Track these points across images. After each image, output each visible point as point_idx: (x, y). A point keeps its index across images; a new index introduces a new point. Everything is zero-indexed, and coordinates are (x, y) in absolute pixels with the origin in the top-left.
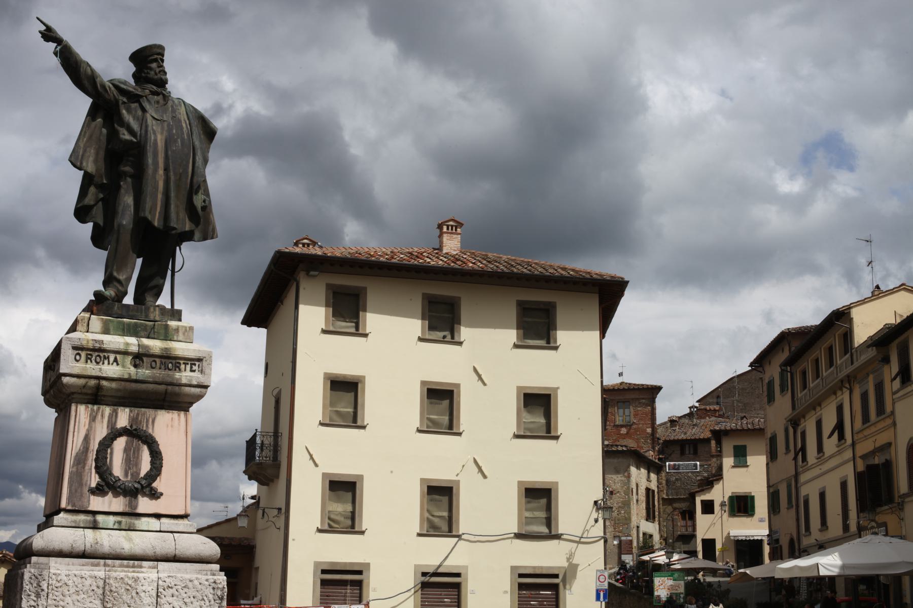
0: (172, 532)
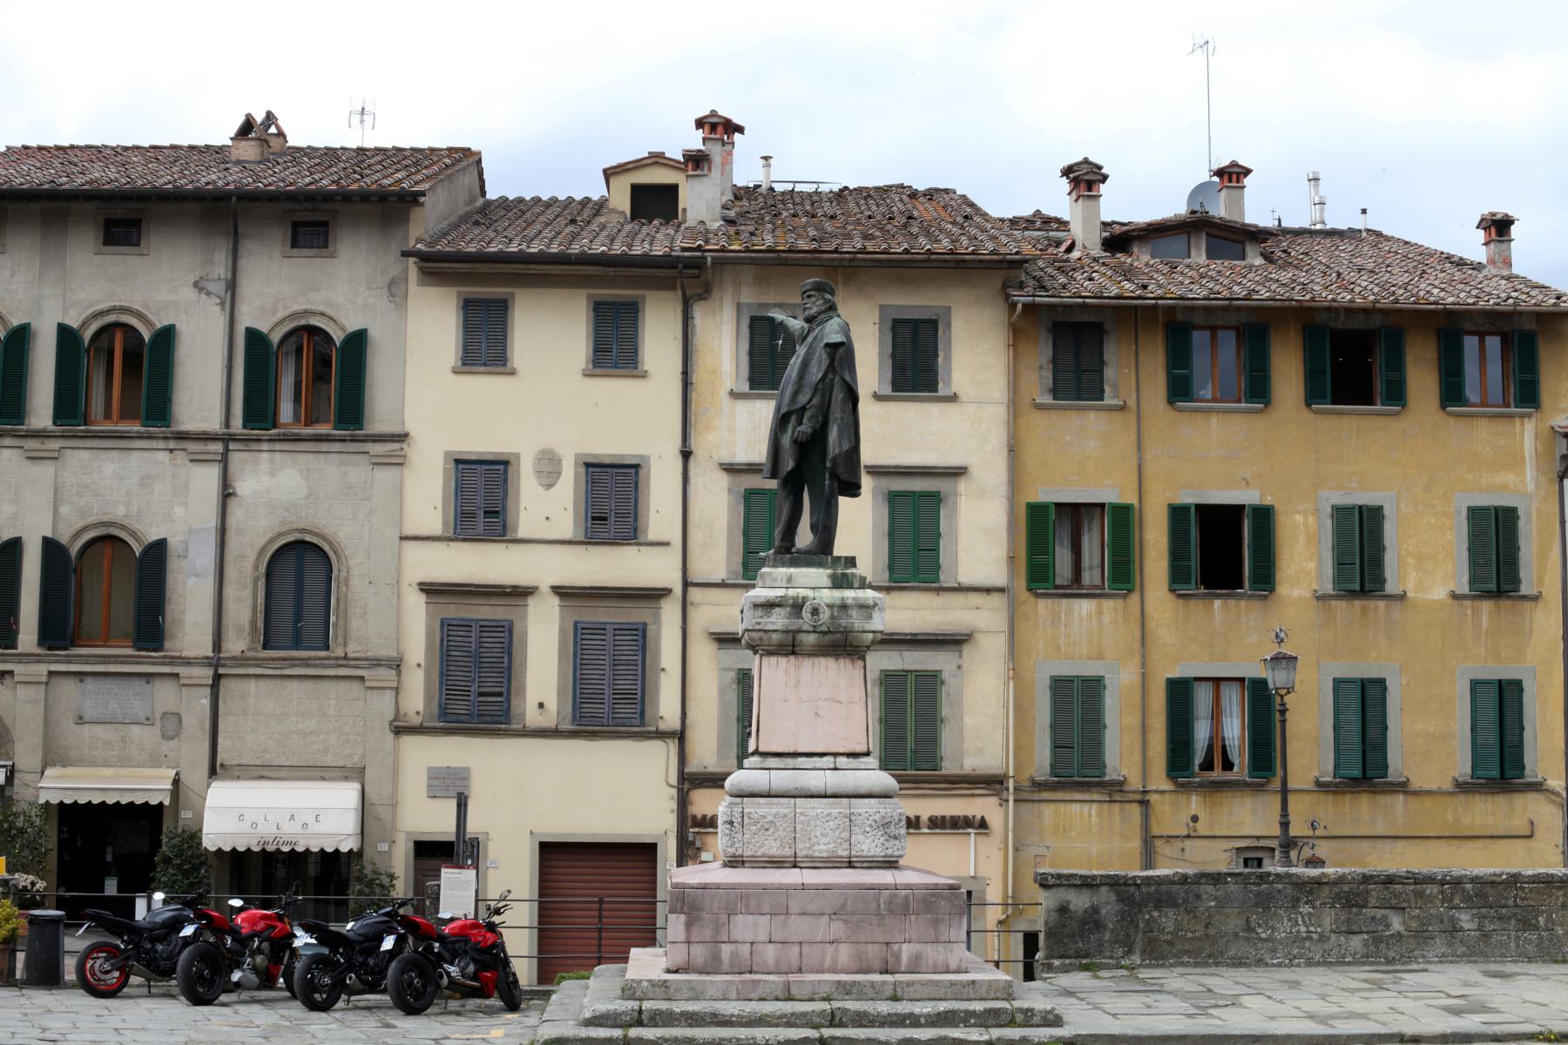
0: (836, 769)
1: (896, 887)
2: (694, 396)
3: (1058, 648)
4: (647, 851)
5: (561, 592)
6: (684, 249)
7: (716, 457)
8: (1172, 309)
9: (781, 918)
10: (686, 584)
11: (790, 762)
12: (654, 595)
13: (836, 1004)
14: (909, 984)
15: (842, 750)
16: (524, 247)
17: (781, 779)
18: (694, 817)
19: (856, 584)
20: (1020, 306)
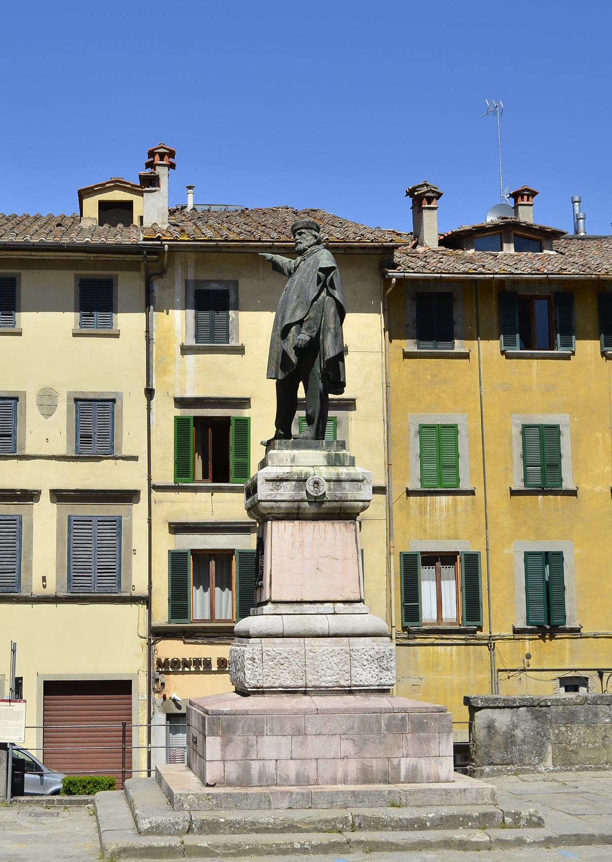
1: (391, 711)
2: (154, 349)
3: (425, 531)
4: (123, 687)
5: (59, 496)
6: (145, 239)
7: (171, 394)
8: (502, 281)
9: (300, 738)
10: (152, 487)
11: (297, 608)
12: (129, 496)
13: (356, 811)
14: (411, 793)
15: (339, 599)
16: (28, 238)
17: (291, 623)
18: (159, 661)
19: (347, 463)
20: (394, 280)
